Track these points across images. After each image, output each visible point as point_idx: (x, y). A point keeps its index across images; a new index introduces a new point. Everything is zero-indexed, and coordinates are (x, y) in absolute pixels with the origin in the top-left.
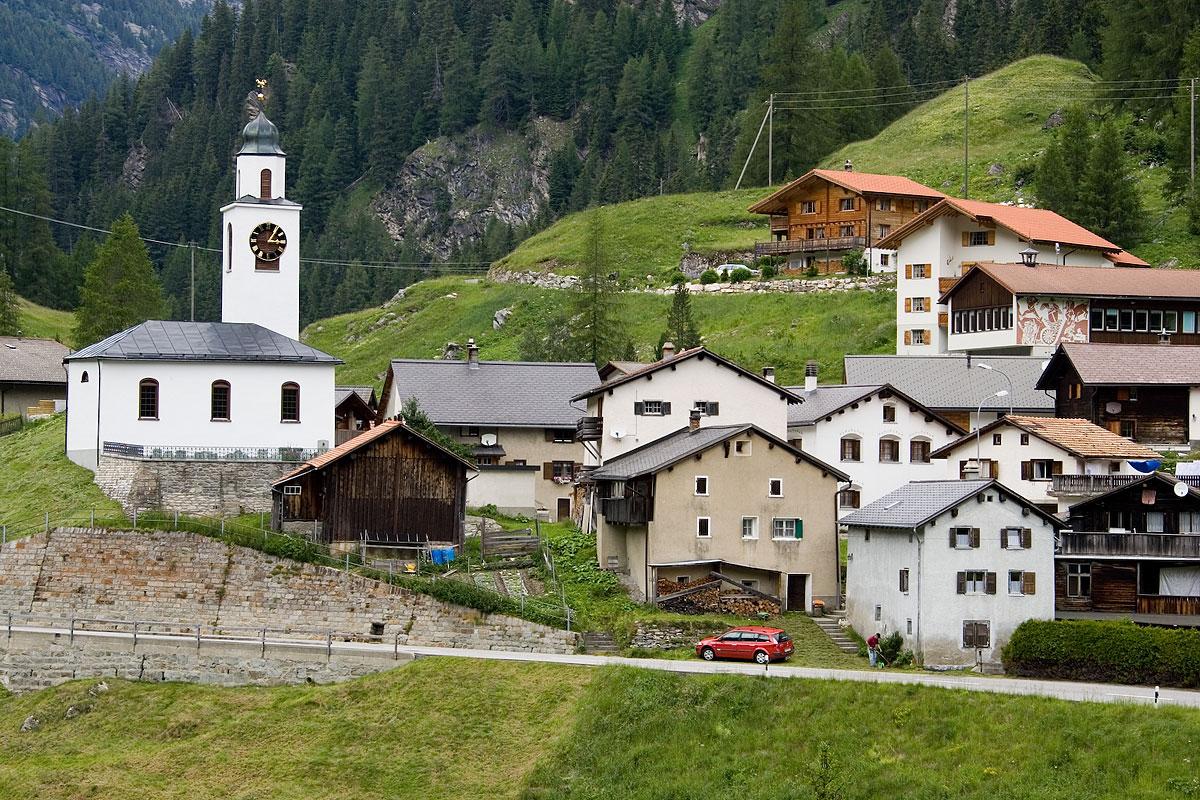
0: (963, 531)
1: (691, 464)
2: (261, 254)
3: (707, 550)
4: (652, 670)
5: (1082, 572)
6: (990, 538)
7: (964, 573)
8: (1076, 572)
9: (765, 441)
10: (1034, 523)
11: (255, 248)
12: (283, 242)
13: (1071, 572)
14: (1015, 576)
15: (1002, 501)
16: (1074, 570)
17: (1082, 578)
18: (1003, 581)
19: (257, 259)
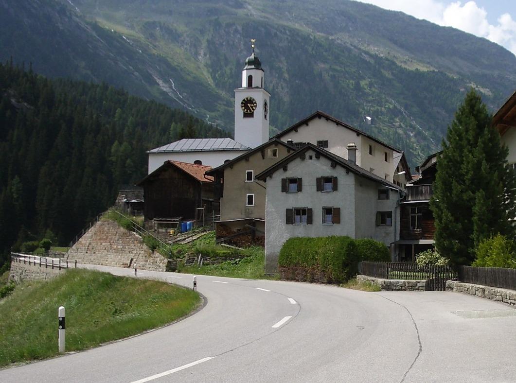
0: (293, 181)
1: (243, 163)
2: (246, 110)
3: (252, 213)
4: (179, 286)
5: (418, 213)
6: (309, 185)
7: (292, 210)
8: (415, 213)
9: (285, 148)
10: (339, 173)
11: (244, 108)
12: (255, 105)
13: (412, 213)
14: (328, 211)
15: (318, 158)
16: (413, 211)
17: (418, 216)
18: (318, 215)
19: (244, 113)
